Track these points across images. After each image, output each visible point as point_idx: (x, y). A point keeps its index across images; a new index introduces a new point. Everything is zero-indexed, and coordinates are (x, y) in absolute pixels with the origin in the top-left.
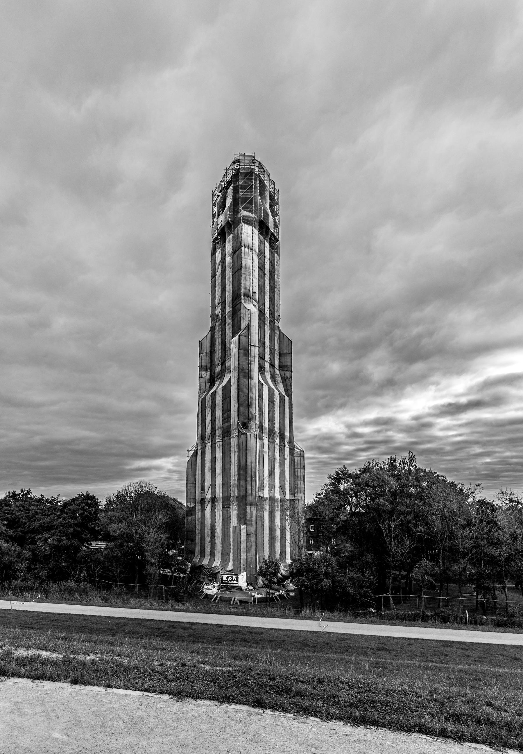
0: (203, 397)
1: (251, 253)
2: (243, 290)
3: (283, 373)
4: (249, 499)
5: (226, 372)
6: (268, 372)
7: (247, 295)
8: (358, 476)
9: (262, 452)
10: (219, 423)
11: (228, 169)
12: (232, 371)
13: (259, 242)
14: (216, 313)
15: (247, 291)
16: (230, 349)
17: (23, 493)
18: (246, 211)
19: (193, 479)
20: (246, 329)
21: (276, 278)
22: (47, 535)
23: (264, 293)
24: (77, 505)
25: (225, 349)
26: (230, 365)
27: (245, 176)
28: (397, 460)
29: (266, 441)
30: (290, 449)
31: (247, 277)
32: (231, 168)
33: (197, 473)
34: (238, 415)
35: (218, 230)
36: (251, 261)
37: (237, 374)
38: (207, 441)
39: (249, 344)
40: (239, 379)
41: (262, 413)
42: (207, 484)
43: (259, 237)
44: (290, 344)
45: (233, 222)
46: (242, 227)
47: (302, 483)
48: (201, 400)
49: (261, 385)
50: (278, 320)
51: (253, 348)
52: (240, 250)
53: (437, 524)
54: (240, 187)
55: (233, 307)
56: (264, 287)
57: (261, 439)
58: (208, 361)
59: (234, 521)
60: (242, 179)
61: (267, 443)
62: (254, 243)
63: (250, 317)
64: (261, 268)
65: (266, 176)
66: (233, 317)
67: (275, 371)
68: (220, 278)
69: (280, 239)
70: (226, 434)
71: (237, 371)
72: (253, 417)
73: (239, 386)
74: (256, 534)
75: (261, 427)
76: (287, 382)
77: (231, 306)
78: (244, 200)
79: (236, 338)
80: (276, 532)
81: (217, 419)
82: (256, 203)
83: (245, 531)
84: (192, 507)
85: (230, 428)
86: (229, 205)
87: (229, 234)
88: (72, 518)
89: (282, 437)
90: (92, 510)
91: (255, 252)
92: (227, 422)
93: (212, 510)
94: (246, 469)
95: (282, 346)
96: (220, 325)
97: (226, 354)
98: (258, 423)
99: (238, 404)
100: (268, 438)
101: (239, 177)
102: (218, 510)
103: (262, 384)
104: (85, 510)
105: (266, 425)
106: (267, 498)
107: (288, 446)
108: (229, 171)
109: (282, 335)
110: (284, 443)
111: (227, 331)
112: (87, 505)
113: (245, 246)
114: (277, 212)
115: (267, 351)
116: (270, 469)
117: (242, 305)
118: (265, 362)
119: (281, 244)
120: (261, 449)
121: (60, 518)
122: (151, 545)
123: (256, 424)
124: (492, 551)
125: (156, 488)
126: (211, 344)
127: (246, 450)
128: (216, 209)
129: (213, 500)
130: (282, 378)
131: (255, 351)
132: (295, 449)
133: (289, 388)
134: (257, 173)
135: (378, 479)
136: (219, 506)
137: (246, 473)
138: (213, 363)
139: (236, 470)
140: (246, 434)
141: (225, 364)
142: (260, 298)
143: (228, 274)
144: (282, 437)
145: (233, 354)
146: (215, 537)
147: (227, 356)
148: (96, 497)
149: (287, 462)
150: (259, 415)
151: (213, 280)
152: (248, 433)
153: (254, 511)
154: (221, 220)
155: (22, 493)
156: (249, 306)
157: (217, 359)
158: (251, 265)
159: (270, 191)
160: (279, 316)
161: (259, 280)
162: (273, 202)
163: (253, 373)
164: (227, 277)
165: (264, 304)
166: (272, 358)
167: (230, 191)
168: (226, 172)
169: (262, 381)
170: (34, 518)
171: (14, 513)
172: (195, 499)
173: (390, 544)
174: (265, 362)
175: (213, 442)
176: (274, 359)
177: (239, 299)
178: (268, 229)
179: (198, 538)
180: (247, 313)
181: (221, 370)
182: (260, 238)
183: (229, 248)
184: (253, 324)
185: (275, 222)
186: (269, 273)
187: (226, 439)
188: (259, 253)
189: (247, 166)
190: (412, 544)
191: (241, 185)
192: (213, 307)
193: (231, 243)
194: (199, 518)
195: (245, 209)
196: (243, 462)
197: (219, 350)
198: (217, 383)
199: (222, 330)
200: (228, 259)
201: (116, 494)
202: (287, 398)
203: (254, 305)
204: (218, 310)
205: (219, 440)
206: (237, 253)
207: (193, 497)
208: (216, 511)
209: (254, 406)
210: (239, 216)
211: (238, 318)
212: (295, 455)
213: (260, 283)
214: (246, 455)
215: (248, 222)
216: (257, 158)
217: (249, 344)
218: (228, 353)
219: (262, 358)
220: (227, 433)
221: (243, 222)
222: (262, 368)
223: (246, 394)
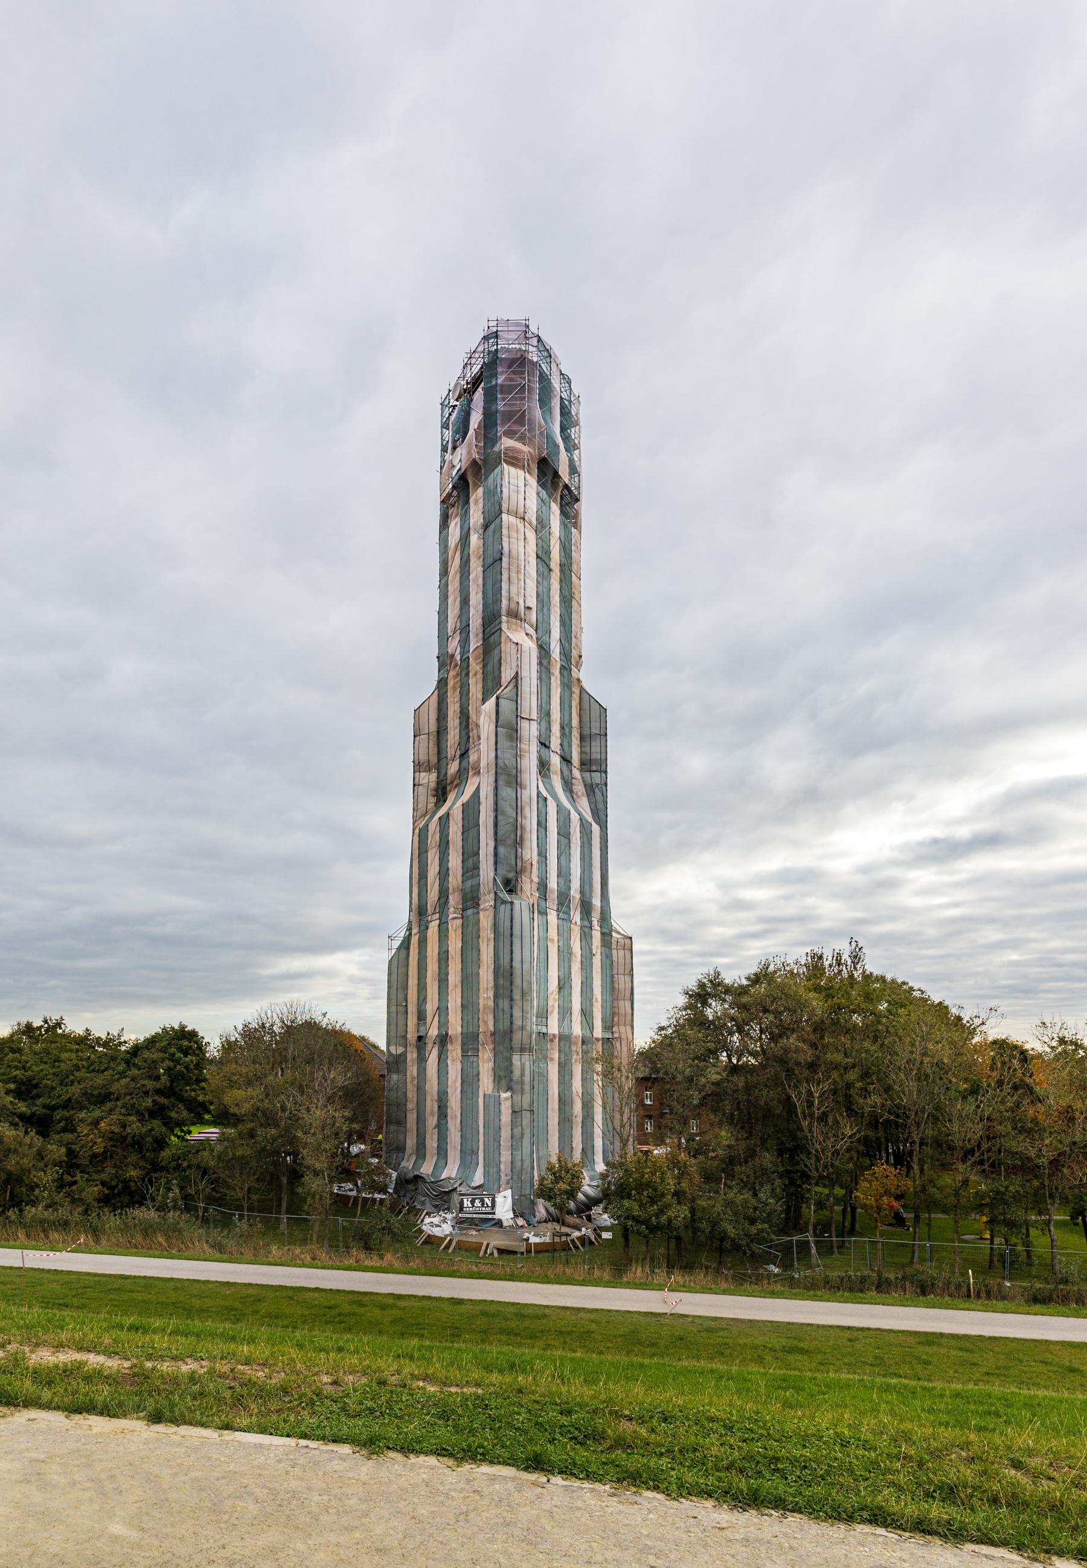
0: (421, 826)
1: (521, 526)
4: (517, 1037)
5: (470, 774)
6: (556, 773)
7: (514, 614)
8: (742, 991)
9: (545, 939)
10: (455, 879)
12: (481, 771)
13: (538, 503)
14: (449, 650)
15: (513, 605)
16: (478, 726)
18: (511, 438)
19: (401, 996)
21: (574, 578)
22: (97, 1113)
27: (510, 367)
28: (825, 956)
29: (552, 917)
31: (514, 575)
34: (496, 863)
36: (522, 543)
37: (492, 779)
39: (517, 716)
40: (496, 788)
42: (431, 1006)
43: (538, 494)
44: (603, 716)
45: (485, 461)
46: (502, 472)
47: (628, 1004)
48: (417, 831)
51: (525, 724)
52: (498, 520)
54: (498, 388)
55: (484, 639)
56: (549, 597)
57: (543, 913)
58: (433, 750)
59: (486, 1084)
60: (502, 373)
62: (527, 506)
63: (519, 659)
64: (543, 557)
65: (553, 365)
66: (483, 660)
67: (571, 771)
68: (458, 578)
69: (584, 498)
71: (494, 771)
72: (526, 868)
73: (496, 803)
74: (532, 1111)
75: (543, 887)
76: (597, 794)
77: (481, 636)
78: (508, 416)
81: (450, 872)
82: (531, 422)
83: (509, 1103)
84: (400, 1055)
86: (476, 427)
87: (476, 487)
88: (150, 1077)
89: (586, 908)
90: (192, 1061)
92: (472, 877)
94: (511, 975)
95: (586, 719)
96: (457, 675)
97: (469, 737)
98: (536, 879)
99: (496, 840)
101: (496, 369)
102: (453, 1061)
103: (545, 799)
105: (553, 883)
106: (554, 1035)
107: (599, 928)
108: (477, 355)
109: (585, 697)
110: (591, 922)
111: (472, 689)
112: (181, 1049)
113: (508, 512)
114: (576, 441)
115: (556, 729)
116: (562, 976)
118: (551, 754)
119: (586, 508)
120: (541, 935)
121: (125, 1077)
125: (324, 1015)
126: (439, 716)
127: (512, 935)
128: (448, 435)
129: (443, 1040)
130: (585, 786)
131: (530, 731)
132: (614, 934)
133: (601, 806)
134: (535, 359)
136: (455, 1051)
139: (491, 977)
140: (512, 903)
141: (468, 756)
142: (540, 620)
144: (586, 908)
145: (483, 736)
146: (446, 1116)
147: (471, 740)
149: (597, 961)
151: (443, 581)
153: (527, 1064)
154: (460, 458)
156: (518, 636)
157: (451, 747)
160: (580, 657)
161: (538, 582)
162: (568, 421)
164: (471, 577)
165: (549, 632)
166: (566, 744)
167: (479, 395)
169: (545, 793)
170: (72, 1077)
171: (30, 1068)
172: (405, 1037)
174: (551, 754)
175: (443, 920)
176: (570, 746)
177: (497, 622)
178: (556, 474)
179: (411, 1118)
180: (514, 651)
182: (541, 495)
184: (525, 673)
185: (571, 463)
186: (558, 567)
187: (469, 912)
188: (539, 526)
189: (514, 346)
190: (857, 1131)
191: (502, 386)
192: (443, 638)
193: (481, 505)
194: (413, 1078)
195: (510, 434)
196: (505, 961)
197: (455, 728)
198: (451, 797)
200: (474, 539)
201: (240, 1028)
203: (527, 634)
204: (454, 645)
205: (455, 915)
208: (449, 1062)
210: (496, 449)
212: (614, 946)
213: (541, 588)
215: (514, 461)
216: (533, 329)
217: (517, 716)
219: (544, 745)
220: (471, 900)
221: (505, 461)
222: (544, 766)
223: (512, 820)
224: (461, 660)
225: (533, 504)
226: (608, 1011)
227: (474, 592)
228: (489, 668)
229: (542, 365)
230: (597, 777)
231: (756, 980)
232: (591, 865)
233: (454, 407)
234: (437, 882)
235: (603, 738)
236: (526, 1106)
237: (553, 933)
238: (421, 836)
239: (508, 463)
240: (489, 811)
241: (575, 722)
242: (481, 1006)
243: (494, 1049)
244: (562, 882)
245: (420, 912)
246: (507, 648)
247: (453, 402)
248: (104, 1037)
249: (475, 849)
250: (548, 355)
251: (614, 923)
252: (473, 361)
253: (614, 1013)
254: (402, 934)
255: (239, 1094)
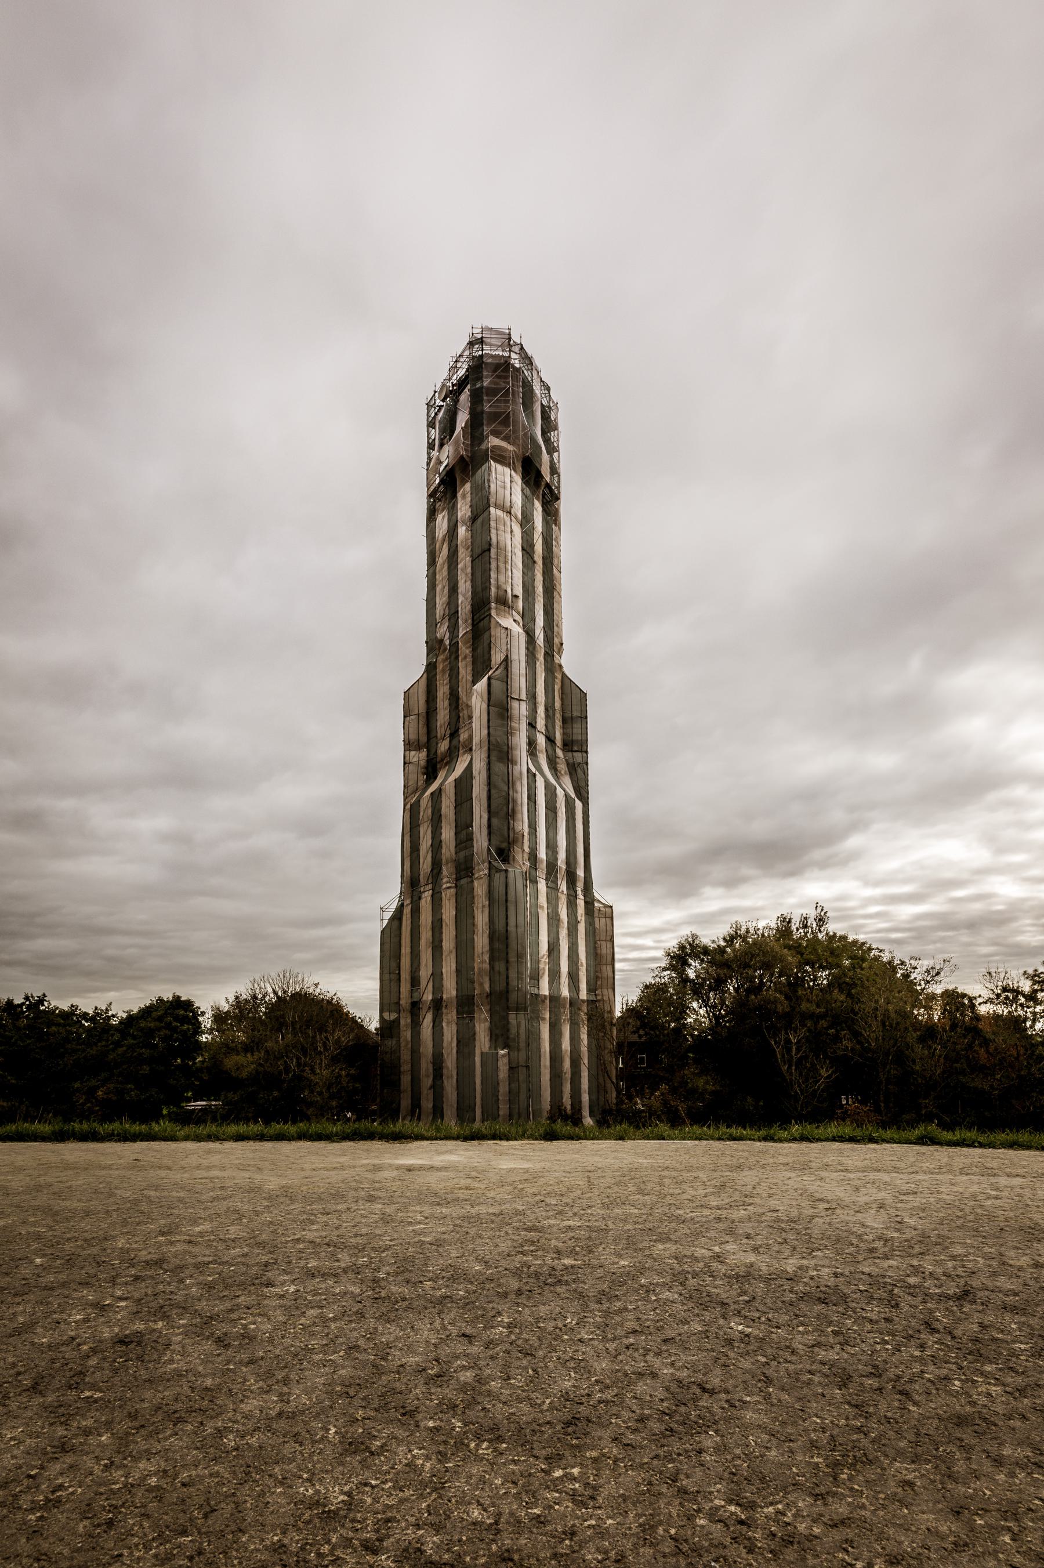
0: (412, 802)
1: (507, 519)
2: (493, 590)
3: (570, 754)
4: (513, 997)
5: (461, 752)
6: (542, 752)
7: (502, 601)
8: (721, 950)
9: (536, 906)
10: (449, 848)
11: (460, 356)
12: (474, 748)
13: (522, 499)
14: (438, 635)
15: (501, 593)
16: (469, 706)
17: (30, 1002)
18: (497, 437)
19: (394, 964)
20: (502, 666)
21: (555, 570)
22: (94, 1082)
23: (534, 599)
24: (155, 1020)
25: (457, 707)
26: (471, 738)
27: (495, 371)
28: (793, 921)
29: (542, 885)
30: (586, 902)
31: (501, 565)
32: (465, 354)
33: (403, 951)
34: (489, 834)
35: (440, 474)
36: (508, 536)
37: (484, 755)
38: (422, 889)
39: (508, 696)
40: (489, 763)
41: (533, 831)
42: (425, 972)
43: (522, 490)
44: (583, 701)
45: (472, 458)
47: (609, 968)
48: (408, 806)
49: (532, 776)
50: (560, 652)
51: (515, 704)
52: (486, 514)
53: (873, 1033)
54: (484, 391)
55: (473, 625)
56: (533, 587)
57: (535, 882)
58: (423, 730)
59: (483, 1041)
61: (545, 889)
62: (513, 501)
63: (509, 643)
64: (528, 549)
65: (535, 373)
66: (473, 644)
68: (446, 568)
69: (563, 496)
70: (463, 873)
72: (517, 838)
73: (489, 777)
75: (533, 857)
76: (579, 774)
77: (470, 621)
78: (494, 416)
79: (482, 685)
80: (564, 1064)
81: (443, 844)
82: (516, 423)
83: (506, 1060)
84: (394, 1021)
85: (472, 860)
86: (463, 425)
87: (464, 483)
90: (188, 1029)
91: (516, 518)
92: (466, 848)
93: (437, 1023)
94: (507, 938)
95: (567, 702)
96: (446, 659)
97: (459, 717)
98: (527, 849)
99: (489, 812)
100: (547, 880)
101: (481, 372)
103: (535, 775)
104: (174, 1030)
105: (542, 854)
106: (545, 996)
107: (582, 897)
108: (462, 360)
109: (566, 680)
110: (576, 892)
111: (462, 671)
112: (177, 1018)
113: (496, 506)
114: (555, 445)
115: (541, 710)
117: (492, 620)
118: (538, 734)
119: (565, 506)
120: (533, 901)
121: (122, 1046)
122: (320, 1093)
123: (524, 851)
124: (978, 1083)
125: (316, 985)
126: (428, 698)
127: (507, 901)
128: (435, 434)
129: (437, 1005)
130: (568, 764)
131: (520, 710)
132: (596, 904)
134: (517, 365)
135: (763, 952)
136: (450, 1016)
137: (507, 948)
138: (433, 735)
139: (486, 941)
140: (506, 871)
143: (462, 560)
145: (476, 715)
146: (442, 1076)
147: (461, 720)
148: (196, 1005)
149: (582, 928)
150: (529, 834)
151: (431, 571)
152: (509, 869)
153: (523, 1022)
154: (446, 455)
155: (28, 1003)
156: (507, 622)
157: (441, 727)
158: (509, 542)
159: (542, 404)
160: (562, 644)
161: (523, 572)
162: (549, 426)
163: (517, 753)
164: (459, 566)
165: (534, 620)
167: (465, 397)
168: (456, 361)
169: (533, 770)
172: (398, 1003)
173: (791, 1074)
174: (538, 734)
175: (437, 889)
176: (554, 727)
177: (486, 609)
178: (539, 475)
179: (406, 1080)
180: (503, 636)
181: (449, 748)
182: (525, 492)
183: (463, 509)
184: (514, 656)
187: (463, 881)
188: (524, 521)
190: (833, 1072)
191: (488, 389)
192: (431, 624)
193: (469, 499)
194: (407, 1042)
195: (496, 434)
196: (500, 926)
197: (445, 709)
198: (442, 775)
199: (451, 670)
200: (462, 531)
201: (231, 999)
202: (579, 804)
203: (515, 621)
204: (443, 631)
205: (449, 885)
206: (480, 520)
207: (394, 999)
208: (444, 1024)
209: (519, 816)
210: (483, 447)
211: (486, 644)
212: (596, 914)
214: (507, 911)
215: (501, 458)
216: (515, 338)
217: (508, 696)
218: (463, 714)
219: (532, 725)
220: (465, 869)
221: (492, 458)
222: (532, 744)
223: (504, 794)
224: (450, 644)
225: (518, 500)
226: (592, 975)
227: (463, 581)
228: (479, 651)
229: (525, 372)
230: (578, 756)
231: (730, 940)
232: (575, 838)
233: (441, 407)
234: (430, 854)
235: (584, 720)
236: (522, 1062)
237: (543, 900)
238: (412, 814)
239: (496, 461)
240: (482, 786)
241: (558, 705)
242: (476, 969)
243: (490, 1009)
244: (550, 853)
245: (412, 884)
246: (497, 634)
247: (439, 402)
248: (91, 1012)
249: (469, 822)
250: (528, 360)
251: (595, 894)
252: (459, 365)
253: (597, 977)
254: (394, 905)
255: (240, 1059)
